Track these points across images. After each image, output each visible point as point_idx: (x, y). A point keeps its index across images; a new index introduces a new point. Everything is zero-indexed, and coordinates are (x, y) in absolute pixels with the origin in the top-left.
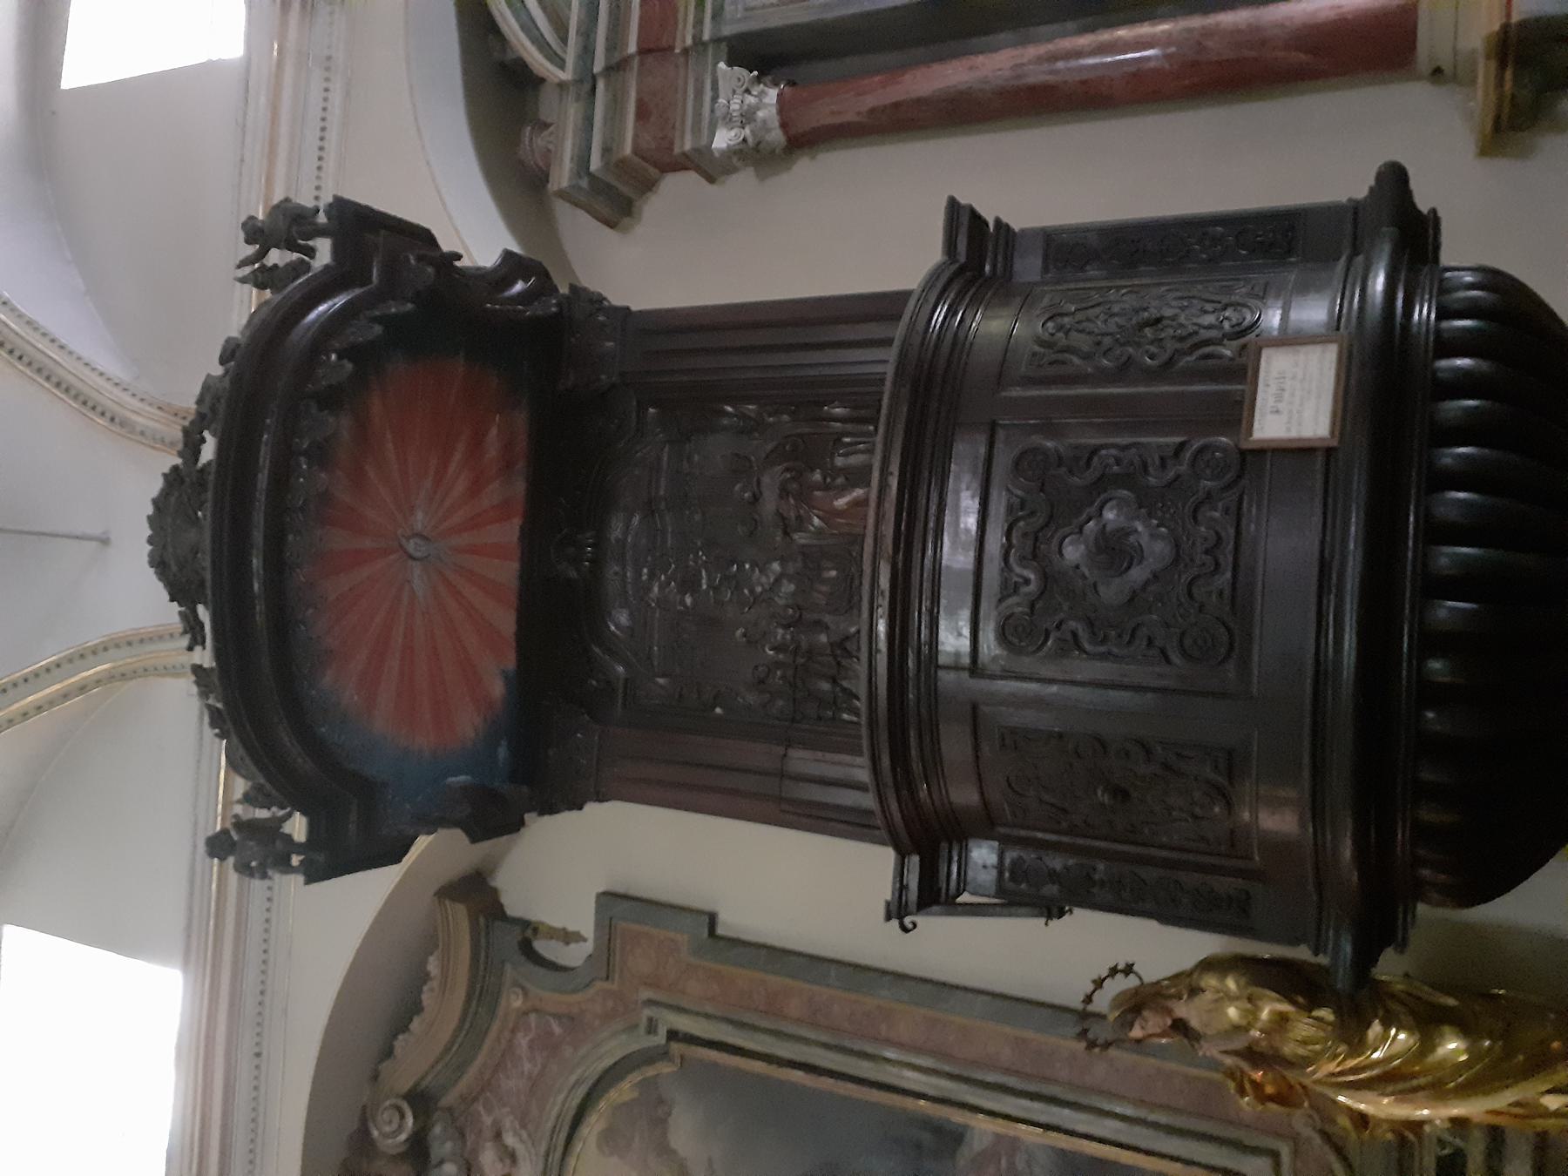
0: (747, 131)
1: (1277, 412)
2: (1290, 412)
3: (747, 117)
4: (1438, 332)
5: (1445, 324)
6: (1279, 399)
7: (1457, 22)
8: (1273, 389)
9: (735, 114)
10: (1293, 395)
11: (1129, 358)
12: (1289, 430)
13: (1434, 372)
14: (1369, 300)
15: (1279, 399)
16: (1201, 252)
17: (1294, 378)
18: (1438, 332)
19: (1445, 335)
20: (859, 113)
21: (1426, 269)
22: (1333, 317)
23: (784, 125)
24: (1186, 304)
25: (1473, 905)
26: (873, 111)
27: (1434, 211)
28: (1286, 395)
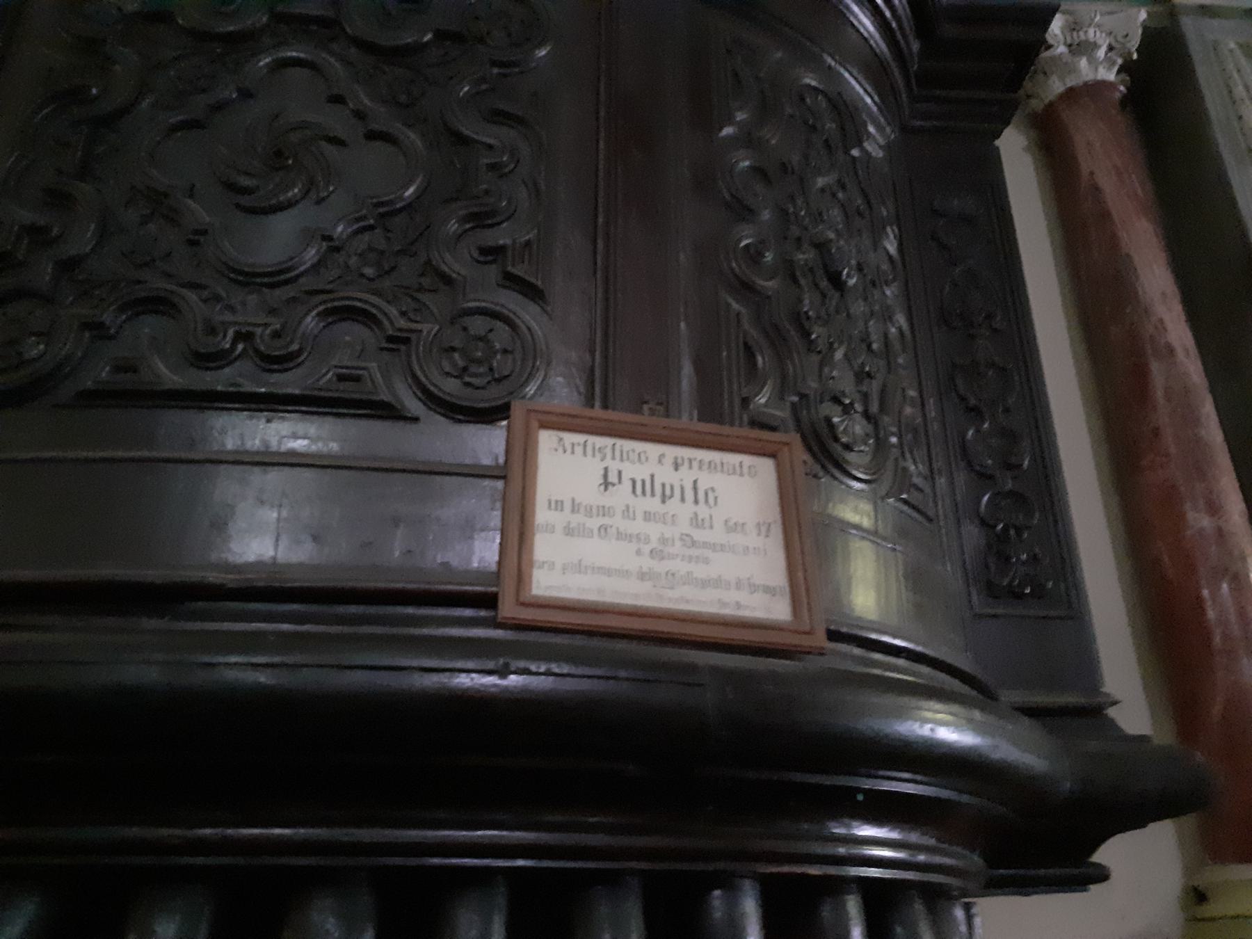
0: (1062, 49)
1: (606, 484)
2: (604, 511)
3: (1081, 48)
4: (837, 886)
5: (853, 905)
6: (641, 488)
7: (660, 682)
8: (666, 475)
9: (1081, 33)
10: (648, 516)
11: (751, 211)
12: (558, 505)
13: (728, 883)
14: (890, 700)
15: (641, 488)
16: (978, 431)
17: (696, 522)
18: (837, 886)
19: (826, 912)
20: (1092, 173)
21: (976, 860)
22: (862, 628)
23: (1071, 95)
24: (875, 346)
25: (1145, 735)
26: (1096, 189)
27: (1101, 875)
28: (653, 504)
